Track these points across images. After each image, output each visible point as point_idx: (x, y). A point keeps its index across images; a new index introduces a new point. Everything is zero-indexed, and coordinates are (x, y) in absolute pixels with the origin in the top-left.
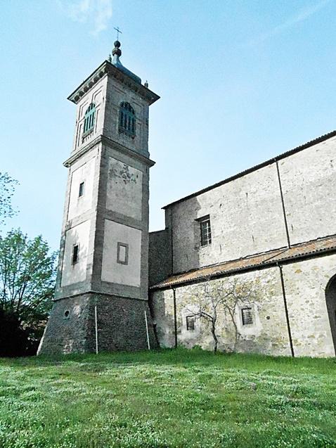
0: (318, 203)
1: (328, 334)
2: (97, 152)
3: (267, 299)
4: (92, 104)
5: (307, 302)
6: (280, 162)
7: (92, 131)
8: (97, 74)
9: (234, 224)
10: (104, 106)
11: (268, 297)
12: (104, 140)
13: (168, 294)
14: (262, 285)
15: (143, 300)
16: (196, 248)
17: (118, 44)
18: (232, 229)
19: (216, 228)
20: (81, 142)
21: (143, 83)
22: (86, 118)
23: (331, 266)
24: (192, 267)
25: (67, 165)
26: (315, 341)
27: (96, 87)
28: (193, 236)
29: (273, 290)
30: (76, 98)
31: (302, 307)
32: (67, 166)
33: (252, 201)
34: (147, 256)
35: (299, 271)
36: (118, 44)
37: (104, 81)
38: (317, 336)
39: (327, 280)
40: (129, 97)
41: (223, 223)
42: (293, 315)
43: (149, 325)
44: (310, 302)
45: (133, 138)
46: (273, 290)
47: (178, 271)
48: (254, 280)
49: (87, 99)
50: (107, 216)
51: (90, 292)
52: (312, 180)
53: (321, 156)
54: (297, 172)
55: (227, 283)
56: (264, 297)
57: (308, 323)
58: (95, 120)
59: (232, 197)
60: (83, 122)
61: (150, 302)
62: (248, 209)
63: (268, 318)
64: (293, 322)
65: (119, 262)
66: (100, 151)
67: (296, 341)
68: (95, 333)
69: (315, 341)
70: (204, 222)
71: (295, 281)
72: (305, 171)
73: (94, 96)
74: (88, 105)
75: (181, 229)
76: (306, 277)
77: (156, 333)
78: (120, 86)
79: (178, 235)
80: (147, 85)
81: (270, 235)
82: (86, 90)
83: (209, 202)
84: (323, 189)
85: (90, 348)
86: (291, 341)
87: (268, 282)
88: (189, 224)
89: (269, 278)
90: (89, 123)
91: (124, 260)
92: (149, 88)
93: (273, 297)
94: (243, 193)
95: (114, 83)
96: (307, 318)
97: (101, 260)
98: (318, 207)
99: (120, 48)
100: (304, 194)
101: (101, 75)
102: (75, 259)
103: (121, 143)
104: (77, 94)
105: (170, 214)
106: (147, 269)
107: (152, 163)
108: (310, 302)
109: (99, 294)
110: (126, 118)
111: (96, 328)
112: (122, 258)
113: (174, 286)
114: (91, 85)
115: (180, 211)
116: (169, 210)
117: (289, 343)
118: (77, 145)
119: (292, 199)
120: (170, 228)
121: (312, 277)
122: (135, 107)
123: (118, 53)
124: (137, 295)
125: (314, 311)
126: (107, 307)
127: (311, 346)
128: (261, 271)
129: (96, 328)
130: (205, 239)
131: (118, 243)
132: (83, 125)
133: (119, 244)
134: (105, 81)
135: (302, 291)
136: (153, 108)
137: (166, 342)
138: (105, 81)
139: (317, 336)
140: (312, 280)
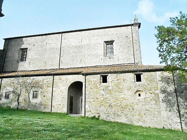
0: (74, 54)
3: (45, 89)
6: (63, 34)
14: (45, 83)
18: (37, 57)
19: (30, 55)
24: (14, 70)
26: (61, 107)
29: (49, 85)
33: (48, 47)
35: (60, 79)
38: (62, 105)
39: (70, 84)
42: (55, 96)
46: (49, 85)
63: (44, 96)
64: (54, 99)
69: (61, 107)
70: (25, 50)
79: (9, 54)
86: (52, 106)
87: (47, 82)
89: (48, 80)
93: (48, 88)
94: (45, 43)
108: (62, 92)
115: (13, 43)
121: (65, 82)
130: (23, 58)
139: (62, 105)
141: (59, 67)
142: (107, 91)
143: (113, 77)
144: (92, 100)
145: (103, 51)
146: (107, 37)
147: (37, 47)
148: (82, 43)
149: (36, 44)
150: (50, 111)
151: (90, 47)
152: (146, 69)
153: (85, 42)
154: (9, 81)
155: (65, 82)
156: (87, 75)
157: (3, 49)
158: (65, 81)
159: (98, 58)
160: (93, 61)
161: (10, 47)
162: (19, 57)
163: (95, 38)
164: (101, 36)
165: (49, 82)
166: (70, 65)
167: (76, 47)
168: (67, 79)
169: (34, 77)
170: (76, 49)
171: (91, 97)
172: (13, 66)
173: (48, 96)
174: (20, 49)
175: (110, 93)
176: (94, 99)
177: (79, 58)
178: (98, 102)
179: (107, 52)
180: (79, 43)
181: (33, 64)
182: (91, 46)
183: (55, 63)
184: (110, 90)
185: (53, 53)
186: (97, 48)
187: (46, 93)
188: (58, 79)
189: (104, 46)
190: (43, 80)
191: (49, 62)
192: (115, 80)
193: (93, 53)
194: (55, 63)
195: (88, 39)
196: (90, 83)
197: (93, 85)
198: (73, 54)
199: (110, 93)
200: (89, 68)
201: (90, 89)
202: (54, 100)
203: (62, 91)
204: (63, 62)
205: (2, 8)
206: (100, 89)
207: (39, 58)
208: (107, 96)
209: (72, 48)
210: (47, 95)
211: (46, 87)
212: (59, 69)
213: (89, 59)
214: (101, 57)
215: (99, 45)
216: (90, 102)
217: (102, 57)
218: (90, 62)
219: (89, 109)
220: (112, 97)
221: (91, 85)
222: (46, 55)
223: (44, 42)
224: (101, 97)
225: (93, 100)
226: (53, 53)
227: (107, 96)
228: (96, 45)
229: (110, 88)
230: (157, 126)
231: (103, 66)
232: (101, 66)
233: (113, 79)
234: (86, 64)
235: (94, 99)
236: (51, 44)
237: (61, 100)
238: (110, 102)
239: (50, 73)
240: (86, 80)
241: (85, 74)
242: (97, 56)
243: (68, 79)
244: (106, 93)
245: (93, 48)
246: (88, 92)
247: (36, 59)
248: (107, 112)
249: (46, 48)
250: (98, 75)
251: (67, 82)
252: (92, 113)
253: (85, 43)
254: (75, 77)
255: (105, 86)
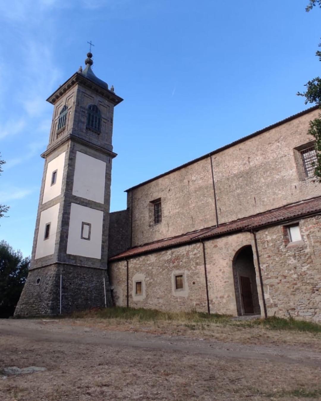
0: (239, 191)
1: (233, 295)
2: (67, 147)
3: (194, 268)
4: (65, 106)
5: (220, 270)
6: (213, 157)
7: (64, 129)
8: (70, 82)
9: (178, 206)
10: (74, 109)
11: (194, 267)
12: (72, 138)
13: (122, 265)
14: (191, 257)
15: (102, 270)
16: (150, 226)
17: (90, 55)
18: (177, 211)
19: (167, 209)
20: (55, 138)
21: (109, 88)
22: (61, 117)
23: (237, 242)
24: (146, 242)
25: (44, 156)
26: (224, 301)
27: (69, 93)
28: (148, 215)
29: (198, 261)
30: (53, 99)
31: (217, 274)
32: (44, 158)
33: (192, 188)
34: (107, 232)
35: (216, 246)
36: (90, 55)
37: (75, 89)
38: (226, 297)
39: (234, 253)
40: (96, 100)
41: (170, 205)
42: (211, 281)
43: (107, 291)
44: (222, 271)
45: (99, 134)
46: (198, 261)
47: (136, 245)
48: (185, 253)
49: (62, 102)
50: (73, 200)
51: (56, 263)
52: (235, 172)
53: (242, 154)
54: (225, 166)
55: (168, 255)
56: (192, 267)
57: (220, 286)
58: (67, 120)
59: (178, 184)
60: (57, 121)
61: (109, 272)
62: (189, 194)
63: (194, 283)
64: (211, 286)
65: (82, 238)
66: (69, 147)
67: (212, 301)
68: (60, 296)
69: (224, 301)
70: (157, 203)
71: (213, 254)
72: (230, 165)
73: (67, 101)
74: (62, 107)
75: (139, 209)
76: (221, 251)
77: (112, 293)
78: (88, 92)
79: (137, 214)
80: (113, 89)
81: (205, 216)
82: (61, 94)
83: (161, 187)
84: (242, 180)
85: (54, 308)
86: (208, 300)
87: (195, 255)
88: (145, 205)
89: (196, 251)
90: (62, 121)
91: (87, 237)
92: (115, 92)
93: (198, 267)
94: (186, 181)
95: (83, 89)
96: (219, 282)
97: (67, 237)
98: (239, 195)
99: (91, 59)
100: (230, 183)
101: (73, 83)
102: (47, 236)
103: (88, 140)
104: (54, 97)
105: (130, 196)
106: (107, 244)
107: (114, 155)
108: (222, 271)
109: (64, 264)
110: (93, 118)
111: (61, 292)
112: (86, 235)
113: (127, 258)
114: (65, 90)
115: (139, 194)
116: (130, 193)
117: (207, 302)
118: (52, 140)
119: (221, 187)
120: (131, 208)
121: (224, 251)
122: (101, 108)
123: (89, 63)
124: (97, 266)
125: (225, 277)
126: (71, 276)
127: (221, 304)
128: (190, 246)
129: (61, 292)
130: (157, 218)
131: (83, 222)
132: (57, 124)
133: (83, 223)
134: (75, 88)
135: (217, 262)
136: (117, 109)
137: (121, 302)
138: (75, 88)
139: (226, 297)
140: (225, 253)
141: (217, 222)
142: (303, 258)
143: (310, 226)
144: (274, 281)
145: (295, 170)
146: (298, 137)
147: (174, 194)
148: (251, 164)
149: (172, 188)
150: (207, 312)
151: (268, 167)
152: (229, 230)
153: (257, 160)
154: (138, 262)
155: (224, 251)
156: (257, 231)
157: (128, 208)
158: (226, 248)
159: (288, 187)
160: (280, 196)
161: (136, 203)
162: (150, 217)
163: (274, 147)
164: (285, 139)
165: (198, 255)
166: (237, 214)
167: (240, 175)
168: (227, 244)
169: (173, 250)
170: (241, 179)
171: (271, 274)
172: (144, 235)
173: (200, 282)
174: (150, 203)
175: (309, 260)
176: (280, 278)
177: (251, 195)
178: (288, 285)
179: (305, 169)
180: (246, 166)
181: (173, 224)
182: (270, 164)
183: (208, 216)
184: (309, 255)
185: (202, 198)
186: (281, 168)
187: (195, 277)
188: (212, 247)
189: (295, 159)
190: (188, 254)
191: (198, 216)
192: (316, 230)
193: (275, 179)
194: (208, 216)
195: (259, 152)
196: (266, 246)
197: (273, 249)
198: (238, 191)
199: (309, 260)
200: (273, 212)
201: (268, 259)
202: (210, 288)
203: (222, 268)
204: (222, 211)
205: (113, 144)
206: (287, 255)
207: (181, 211)
208: (305, 269)
209: (234, 180)
210: (198, 279)
211: (194, 265)
212: (218, 227)
213: (269, 193)
214: (295, 184)
215: (284, 159)
216: (272, 286)
217: (296, 183)
218: (274, 199)
219: (272, 301)
220: (315, 269)
221: (268, 249)
222: (192, 203)
223: (185, 181)
224: (293, 272)
225: (277, 281)
226: (202, 198)
227: (305, 269)
228: (279, 160)
229: (308, 250)
230: (35, 266)
231: (302, 202)
232: (297, 204)
233: (312, 230)
234: (267, 205)
235: (280, 278)
236: (196, 182)
237: (222, 288)
238: (312, 281)
239: (196, 238)
240: (258, 240)
241: (253, 229)
242: (283, 182)
243: (230, 243)
244: (301, 262)
245: (273, 169)
246: (265, 266)
247: (177, 216)
248: (311, 306)
249: (188, 192)
250: (279, 227)
251: (228, 250)
252: (281, 310)
253: (257, 163)
254: (242, 237)
255: (295, 248)
